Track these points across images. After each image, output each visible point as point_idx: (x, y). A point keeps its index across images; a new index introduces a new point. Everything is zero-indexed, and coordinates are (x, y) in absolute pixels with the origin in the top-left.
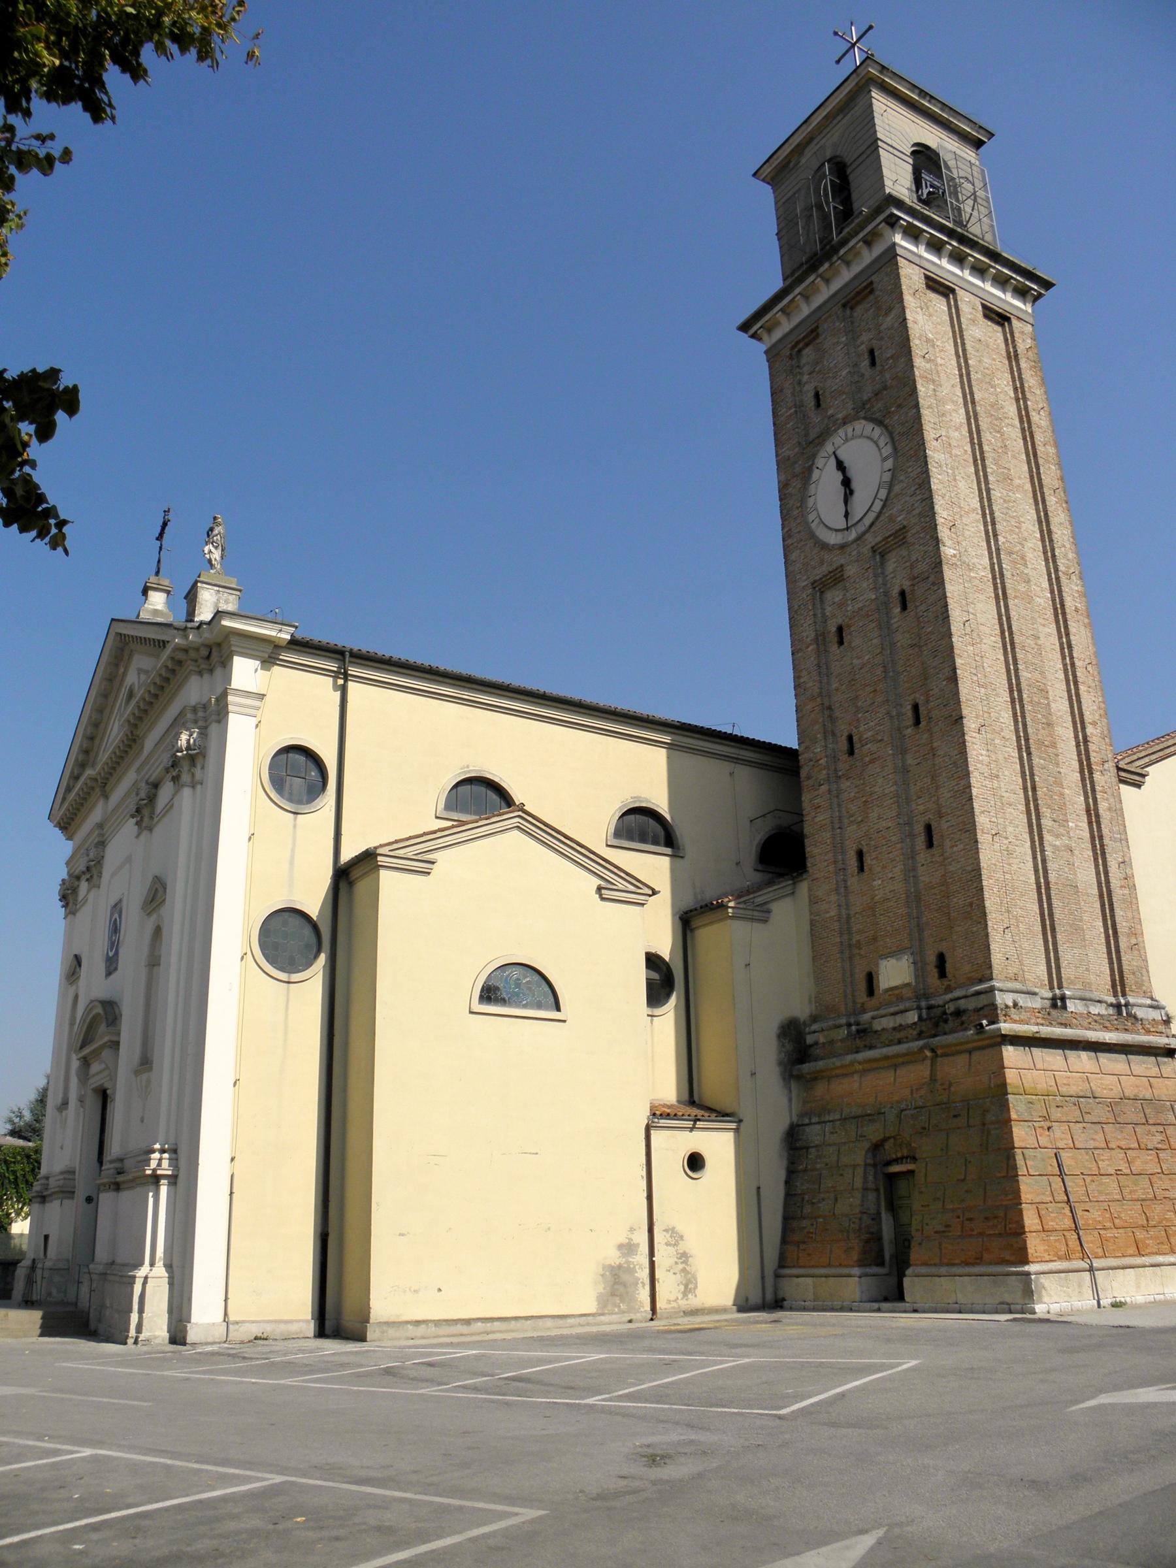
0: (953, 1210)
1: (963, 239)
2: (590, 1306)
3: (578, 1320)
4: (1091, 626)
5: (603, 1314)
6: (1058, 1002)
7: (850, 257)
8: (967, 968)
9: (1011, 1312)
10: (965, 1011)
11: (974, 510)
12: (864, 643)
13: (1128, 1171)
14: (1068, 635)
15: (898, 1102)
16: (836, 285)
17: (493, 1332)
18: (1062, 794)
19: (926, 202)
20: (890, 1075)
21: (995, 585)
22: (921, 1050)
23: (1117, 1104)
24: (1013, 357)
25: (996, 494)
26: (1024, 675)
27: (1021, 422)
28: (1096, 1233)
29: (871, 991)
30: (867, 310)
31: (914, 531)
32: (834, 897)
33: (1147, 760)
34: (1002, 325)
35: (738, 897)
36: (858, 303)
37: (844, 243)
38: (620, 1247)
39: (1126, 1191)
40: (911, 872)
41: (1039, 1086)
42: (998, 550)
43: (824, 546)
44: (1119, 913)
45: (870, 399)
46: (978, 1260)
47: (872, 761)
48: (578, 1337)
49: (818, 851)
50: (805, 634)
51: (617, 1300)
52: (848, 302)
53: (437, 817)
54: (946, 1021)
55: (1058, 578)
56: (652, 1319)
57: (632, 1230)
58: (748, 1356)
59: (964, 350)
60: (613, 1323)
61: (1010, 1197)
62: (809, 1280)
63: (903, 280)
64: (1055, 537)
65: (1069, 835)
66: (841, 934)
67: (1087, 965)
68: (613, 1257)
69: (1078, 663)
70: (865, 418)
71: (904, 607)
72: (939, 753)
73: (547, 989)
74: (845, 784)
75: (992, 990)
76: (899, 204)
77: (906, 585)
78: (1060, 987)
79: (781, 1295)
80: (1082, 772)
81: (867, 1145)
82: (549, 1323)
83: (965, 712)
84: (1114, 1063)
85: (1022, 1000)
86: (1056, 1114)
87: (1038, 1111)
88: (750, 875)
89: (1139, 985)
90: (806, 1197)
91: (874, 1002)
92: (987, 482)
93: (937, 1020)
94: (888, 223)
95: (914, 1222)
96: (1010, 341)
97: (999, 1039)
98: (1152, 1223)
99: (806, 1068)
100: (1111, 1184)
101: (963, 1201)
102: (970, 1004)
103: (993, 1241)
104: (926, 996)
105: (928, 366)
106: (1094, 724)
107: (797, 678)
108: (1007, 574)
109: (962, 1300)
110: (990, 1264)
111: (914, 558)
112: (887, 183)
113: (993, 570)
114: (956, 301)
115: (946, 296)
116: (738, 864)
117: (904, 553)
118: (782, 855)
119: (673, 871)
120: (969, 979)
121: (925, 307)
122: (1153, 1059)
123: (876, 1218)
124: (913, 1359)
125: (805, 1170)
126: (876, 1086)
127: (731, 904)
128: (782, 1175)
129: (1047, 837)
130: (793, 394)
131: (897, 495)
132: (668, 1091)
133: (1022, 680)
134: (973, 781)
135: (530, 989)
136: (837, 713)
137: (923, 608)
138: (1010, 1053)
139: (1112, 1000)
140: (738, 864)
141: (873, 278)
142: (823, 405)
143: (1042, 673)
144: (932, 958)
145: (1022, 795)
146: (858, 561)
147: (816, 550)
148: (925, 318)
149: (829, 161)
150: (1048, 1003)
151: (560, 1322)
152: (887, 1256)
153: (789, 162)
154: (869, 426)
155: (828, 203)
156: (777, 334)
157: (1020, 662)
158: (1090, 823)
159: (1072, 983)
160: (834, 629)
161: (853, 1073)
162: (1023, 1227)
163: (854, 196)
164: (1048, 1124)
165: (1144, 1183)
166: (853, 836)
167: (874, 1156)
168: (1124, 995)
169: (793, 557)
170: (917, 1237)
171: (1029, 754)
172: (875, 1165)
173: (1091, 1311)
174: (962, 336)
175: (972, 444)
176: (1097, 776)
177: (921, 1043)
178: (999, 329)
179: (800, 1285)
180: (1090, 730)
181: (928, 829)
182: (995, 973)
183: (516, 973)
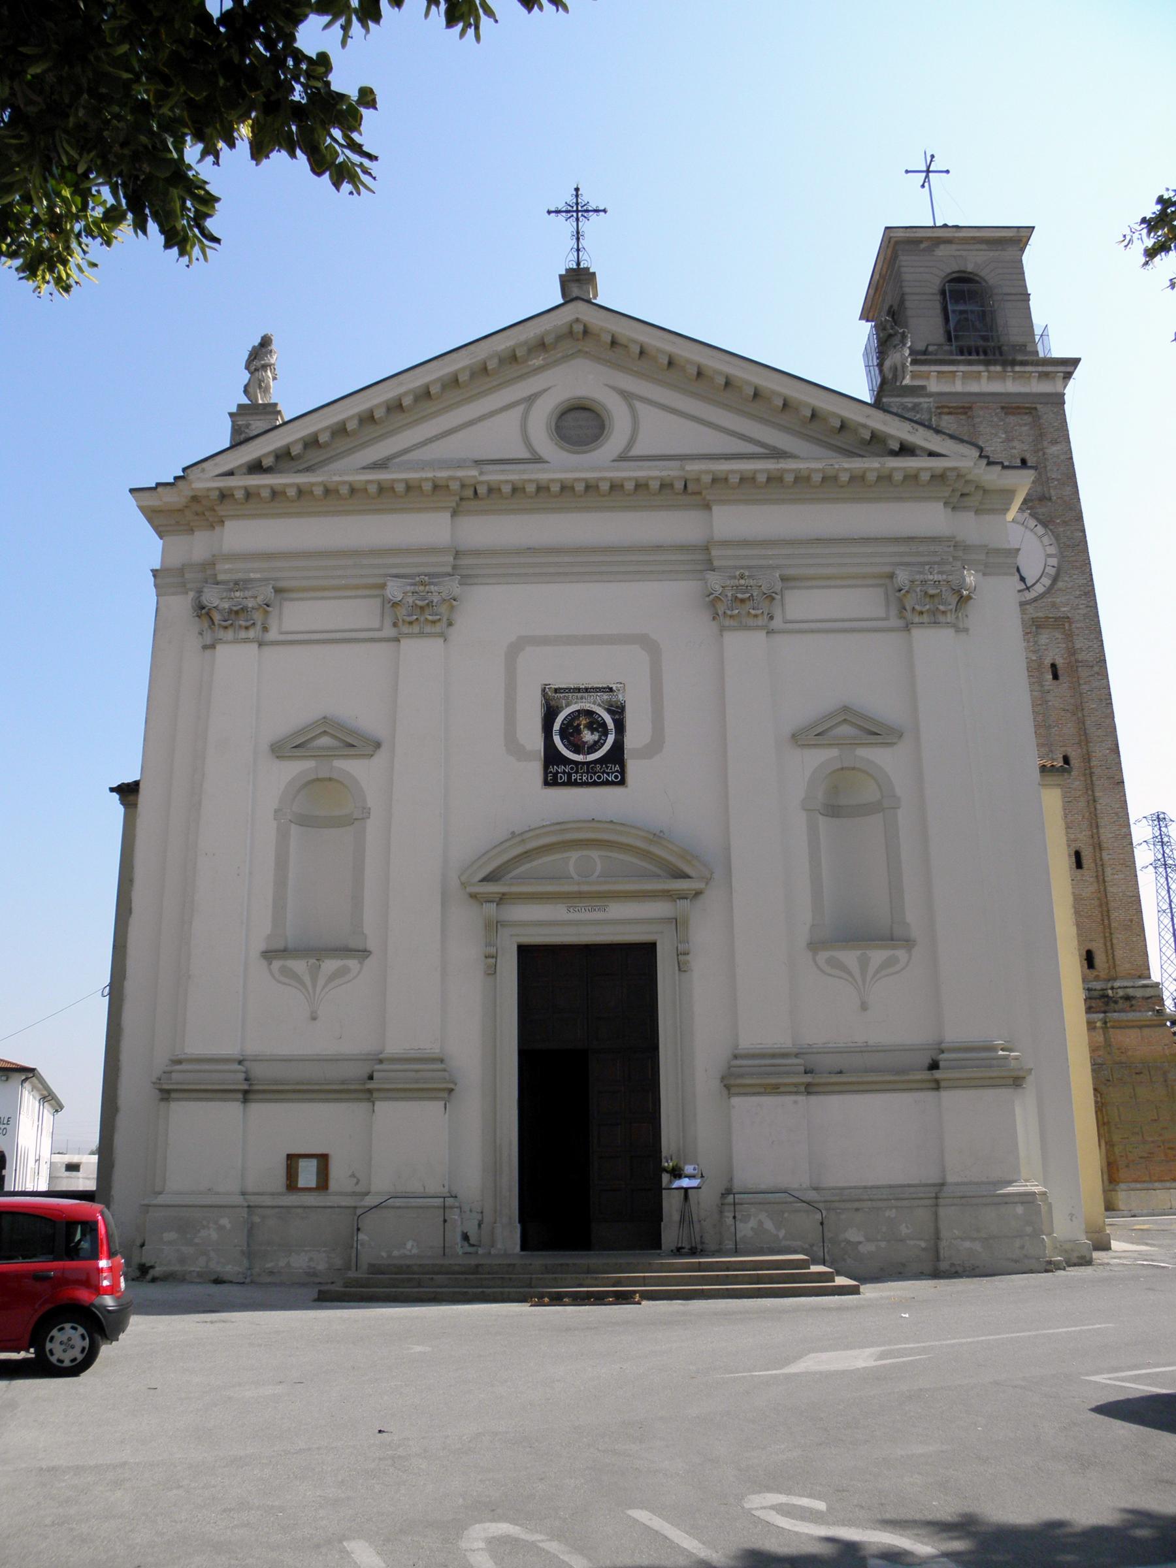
36: (1013, 414)
102: (1139, 993)
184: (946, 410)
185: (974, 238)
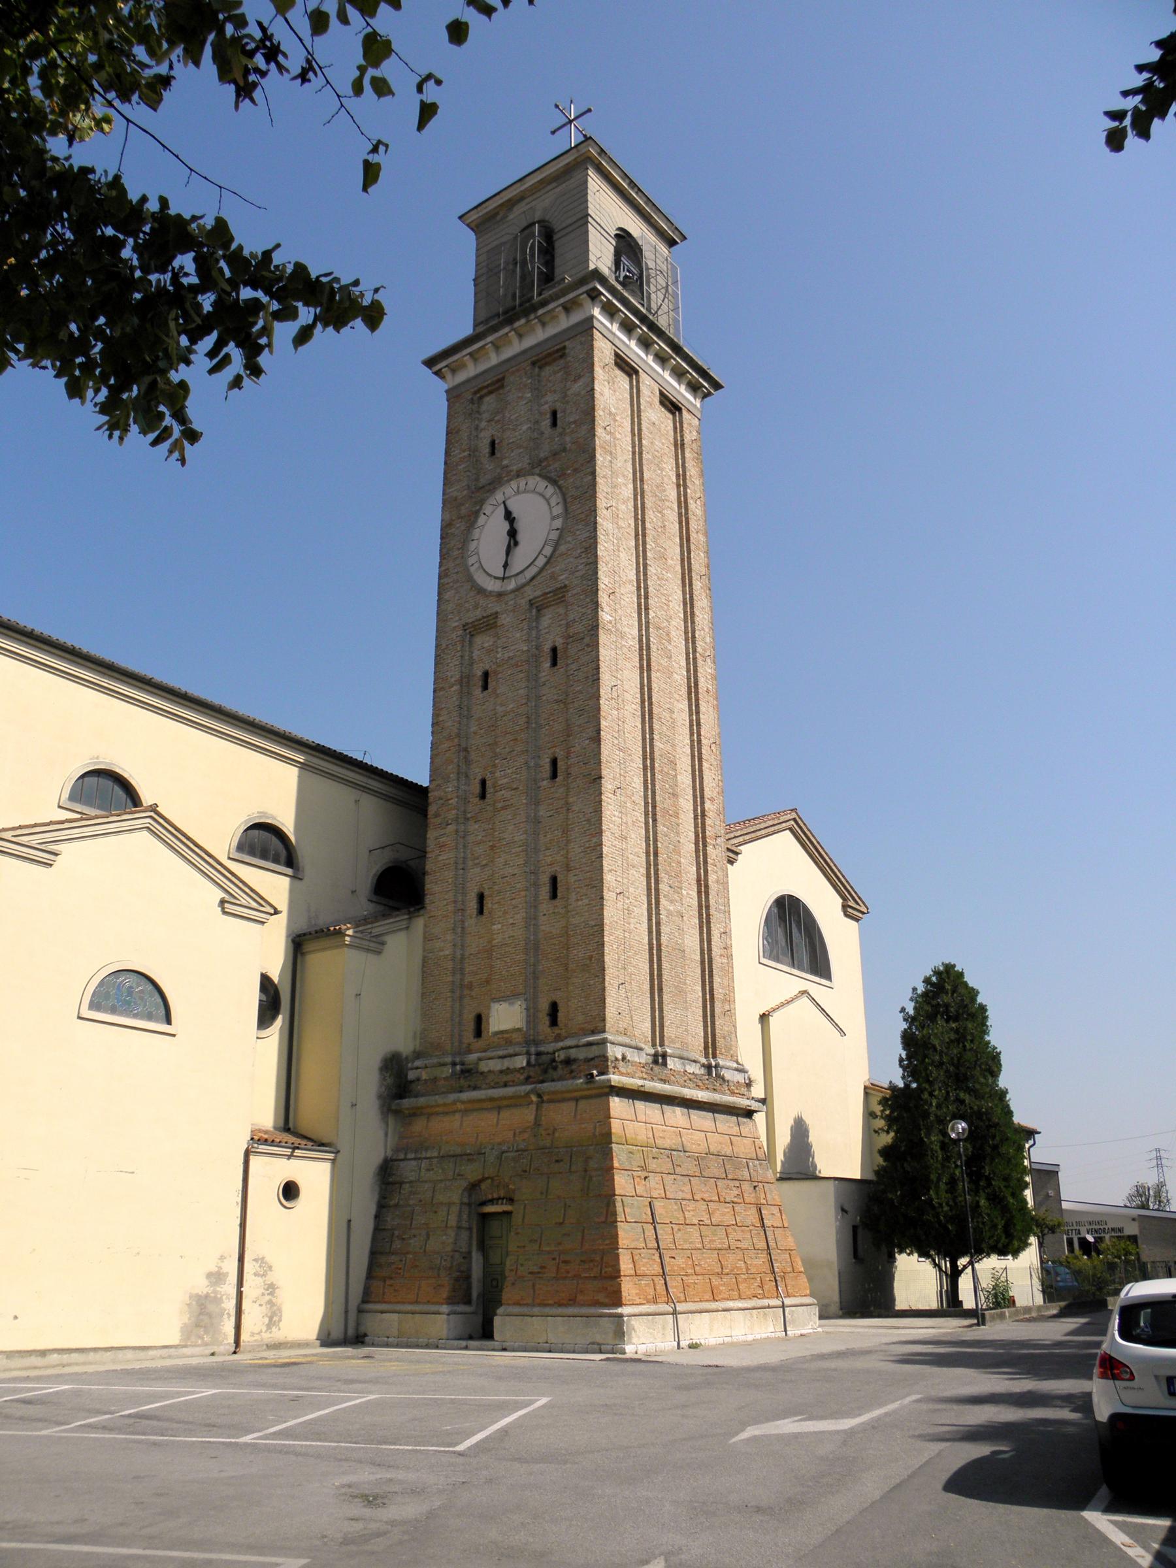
0: (549, 1252)
1: (653, 327)
2: (174, 1338)
3: (164, 1352)
4: (717, 708)
5: (185, 1346)
6: (660, 1059)
7: (547, 319)
8: (581, 1018)
9: (601, 1352)
10: (575, 1060)
11: (631, 581)
12: (510, 691)
13: (708, 1222)
14: (698, 713)
15: (500, 1144)
16: (529, 342)
17: (69, 1365)
18: (679, 862)
19: (623, 284)
20: (492, 1117)
21: (641, 656)
22: (527, 1094)
23: (703, 1158)
24: (679, 445)
25: (651, 570)
26: (658, 744)
27: (679, 507)
28: (679, 1278)
29: (478, 1033)
30: (555, 373)
31: (574, 592)
32: (449, 937)
33: (741, 839)
34: (673, 414)
35: (358, 923)
36: (546, 364)
37: (544, 304)
38: (209, 1275)
39: (706, 1241)
40: (532, 920)
41: (639, 1138)
42: (648, 623)
43: (481, 591)
44: (717, 979)
45: (546, 459)
46: (572, 1302)
47: (503, 808)
48: (168, 1370)
49: (439, 888)
50: (449, 674)
51: (201, 1331)
52: (538, 361)
53: (59, 807)
54: (555, 1068)
55: (695, 659)
56: (235, 1353)
57: (222, 1258)
58: (371, 1393)
59: (640, 430)
60: (196, 1356)
61: (607, 1242)
62: (395, 1316)
63: (596, 351)
64: (697, 619)
65: (680, 903)
66: (454, 974)
67: (685, 1026)
68: (201, 1286)
69: (704, 741)
70: (540, 475)
71: (554, 663)
72: (574, 808)
73: (159, 1000)
74: (473, 827)
75: (604, 1042)
76: (603, 280)
77: (559, 642)
78: (662, 1045)
79: (362, 1330)
80: (697, 844)
81: (464, 1184)
82: (130, 1355)
83: (604, 773)
84: (703, 1120)
85: (632, 1055)
86: (653, 1165)
87: (637, 1161)
88: (364, 905)
89: (728, 1048)
90: (396, 1233)
91: (481, 1043)
92: (645, 558)
93: (546, 1067)
94: (589, 296)
95: (508, 1263)
96: (678, 429)
97: (607, 1090)
98: (726, 1271)
99: (407, 1103)
100: (694, 1232)
101: (560, 1244)
102: (581, 1054)
103: (588, 1282)
104: (536, 1043)
105: (608, 437)
106: (712, 800)
107: (436, 715)
108: (653, 648)
109: (552, 1339)
110: (583, 1305)
111: (571, 617)
112: (592, 257)
113: (640, 641)
114: (638, 382)
115: (630, 375)
116: (353, 892)
117: (561, 611)
118: (399, 888)
119: (292, 891)
120: (582, 1029)
121: (611, 381)
122: (735, 1118)
123: (467, 1256)
124: (544, 1395)
125: (397, 1206)
126: (473, 1126)
127: (350, 932)
128: (373, 1210)
129: (663, 901)
130: (469, 439)
131: (562, 555)
132: (266, 1116)
133: (656, 749)
134: (605, 839)
135: (142, 998)
136: (473, 756)
137: (574, 667)
138: (617, 1104)
139: (704, 1061)
140: (353, 892)
141: (567, 343)
142: (498, 454)
143: (673, 746)
144: (544, 1006)
145: (644, 859)
146: (514, 611)
147: (472, 594)
148: (610, 392)
149: (539, 222)
150: (650, 1059)
151: (142, 1354)
152: (475, 1294)
153: (497, 214)
154: (542, 484)
155: (532, 262)
156: (461, 377)
157: (656, 732)
158: (699, 892)
159: (672, 1041)
160: (479, 673)
161: (455, 1112)
162: (619, 1271)
163: (558, 261)
164: (645, 1174)
165: (721, 1232)
166: (475, 879)
167: (470, 1196)
168: (714, 1057)
169: (447, 596)
170: (510, 1277)
171: (655, 820)
172: (469, 1205)
173: (671, 1352)
174: (639, 416)
175: (636, 519)
176: (709, 849)
177: (529, 1087)
178: (671, 416)
179: (385, 1321)
180: (708, 805)
181: (554, 880)
182: (608, 1026)
183: (129, 981)
184: (485, 391)
185: (541, 182)
